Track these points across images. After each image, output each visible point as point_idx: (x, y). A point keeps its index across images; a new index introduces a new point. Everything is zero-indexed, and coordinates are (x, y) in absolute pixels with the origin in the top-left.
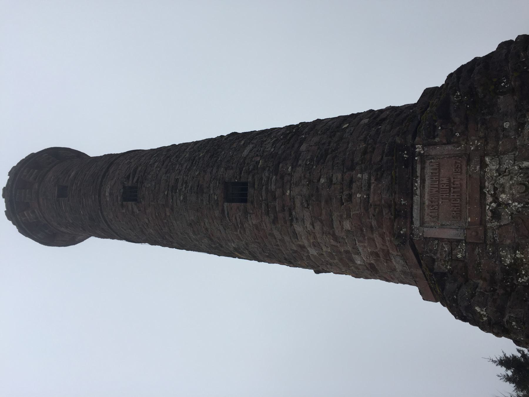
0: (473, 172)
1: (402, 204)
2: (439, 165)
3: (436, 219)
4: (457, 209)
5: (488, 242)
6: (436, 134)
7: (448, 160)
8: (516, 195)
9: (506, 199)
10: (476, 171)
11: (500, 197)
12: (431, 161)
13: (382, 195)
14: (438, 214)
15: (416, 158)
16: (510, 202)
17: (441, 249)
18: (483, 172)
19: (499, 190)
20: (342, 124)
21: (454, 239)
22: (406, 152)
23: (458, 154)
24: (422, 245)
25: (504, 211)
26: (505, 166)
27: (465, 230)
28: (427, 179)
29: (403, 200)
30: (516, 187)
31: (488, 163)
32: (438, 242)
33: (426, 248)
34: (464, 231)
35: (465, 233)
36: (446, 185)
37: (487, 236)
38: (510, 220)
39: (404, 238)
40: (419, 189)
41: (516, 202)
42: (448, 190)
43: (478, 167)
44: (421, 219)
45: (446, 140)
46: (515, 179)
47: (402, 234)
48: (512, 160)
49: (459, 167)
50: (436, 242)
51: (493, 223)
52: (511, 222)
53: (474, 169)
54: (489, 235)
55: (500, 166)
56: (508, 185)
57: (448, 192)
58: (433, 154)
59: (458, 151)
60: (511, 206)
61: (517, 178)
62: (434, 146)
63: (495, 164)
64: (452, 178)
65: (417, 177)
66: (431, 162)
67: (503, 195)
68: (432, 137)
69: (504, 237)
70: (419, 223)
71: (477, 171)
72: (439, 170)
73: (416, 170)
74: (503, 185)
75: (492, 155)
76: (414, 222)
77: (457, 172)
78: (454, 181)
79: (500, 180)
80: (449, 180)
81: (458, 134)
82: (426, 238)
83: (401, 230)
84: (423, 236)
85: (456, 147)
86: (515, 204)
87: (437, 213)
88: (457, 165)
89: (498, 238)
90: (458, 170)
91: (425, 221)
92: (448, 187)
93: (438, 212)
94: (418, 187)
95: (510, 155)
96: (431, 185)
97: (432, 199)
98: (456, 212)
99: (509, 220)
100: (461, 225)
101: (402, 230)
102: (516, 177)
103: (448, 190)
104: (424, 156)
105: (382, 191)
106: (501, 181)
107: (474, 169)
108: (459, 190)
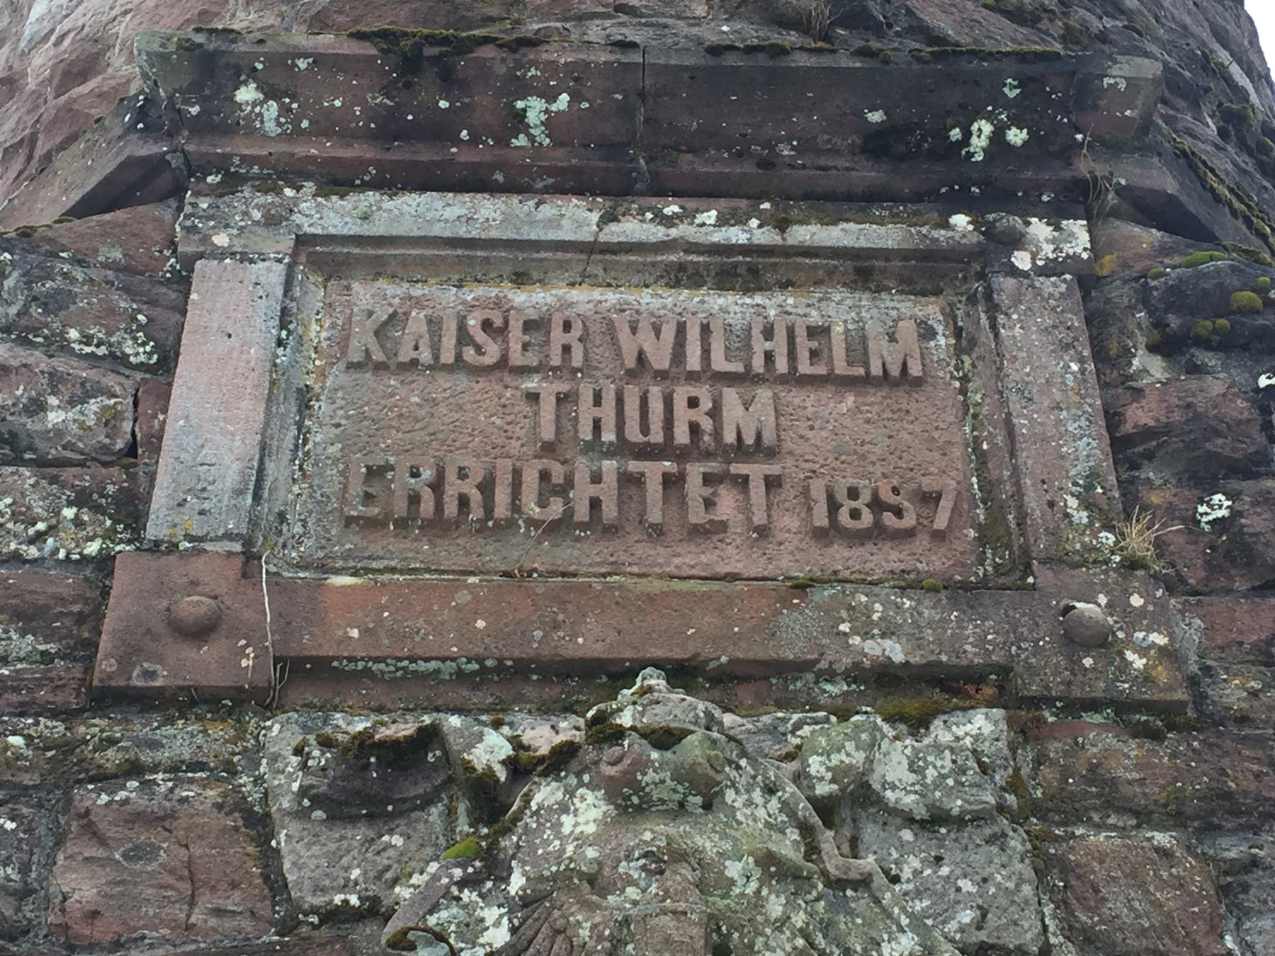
0: (844, 614)
1: (520, 104)
2: (903, 381)
3: (367, 352)
4: (464, 501)
5: (94, 728)
6: (1210, 359)
7: (957, 452)
8: (591, 907)
9: (547, 843)
10: (855, 631)
11: (571, 793)
12: (940, 329)
13: (608, 16)
14: (414, 363)
15: (960, 221)
16: (517, 883)
17: (55, 381)
18: (845, 694)
19: (650, 762)
20: (1159, 155)
21: (152, 477)
22: (1016, 136)
23: (1020, 508)
24: (117, 255)
25: (429, 851)
26: (916, 864)
27: (237, 547)
28: (758, 299)
29: (554, 108)
30: (682, 906)
31: (940, 732)
32: (140, 367)
33: (80, 276)
34: (229, 536)
35: (208, 546)
36: (707, 424)
37: (170, 721)
38: (319, 900)
39: (195, 110)
40: (657, 233)
41: (514, 930)
42: (657, 436)
43: (896, 651)
44: (372, 252)
45: (1152, 423)
46: (776, 907)
47: (231, 98)
48: (979, 925)
49: (888, 519)
50: (138, 352)
51: (295, 760)
52: (296, 908)
53: (875, 617)
54: (168, 730)
55: (909, 820)
56: (707, 843)
57: (633, 433)
58: (1012, 331)
59: (1051, 504)
60: (467, 895)
61: (785, 920)
62: (1084, 338)
63: (931, 773)
64: (774, 469)
65: (782, 225)
66: (927, 333)
67: (595, 813)
68: (1174, 321)
69: (138, 853)
70: (332, 231)
71: (856, 640)
72: (848, 383)
73: (847, 221)
74: (707, 806)
75: (1025, 771)
76: (342, 197)
77: (834, 507)
78: (743, 482)
79: (757, 795)
80: (761, 450)
81: (1218, 507)
82: (183, 281)
83: (270, 93)
84: (201, 256)
85: (1089, 487)
86: (497, 924)
87: (425, 356)
88: (906, 504)
89: (126, 801)
90: (855, 514)
91: (356, 286)
92: (682, 436)
93: (437, 366)
94: (682, 230)
95: (1031, 913)
96: (706, 330)
97: (567, 326)
98: (427, 494)
99: (318, 889)
100: (298, 529)
101: (268, 96)
102: (799, 919)
103: (657, 436)
104: (981, 276)
105: (643, 21)
106: (749, 803)
107: (875, 617)
108: (655, 516)
